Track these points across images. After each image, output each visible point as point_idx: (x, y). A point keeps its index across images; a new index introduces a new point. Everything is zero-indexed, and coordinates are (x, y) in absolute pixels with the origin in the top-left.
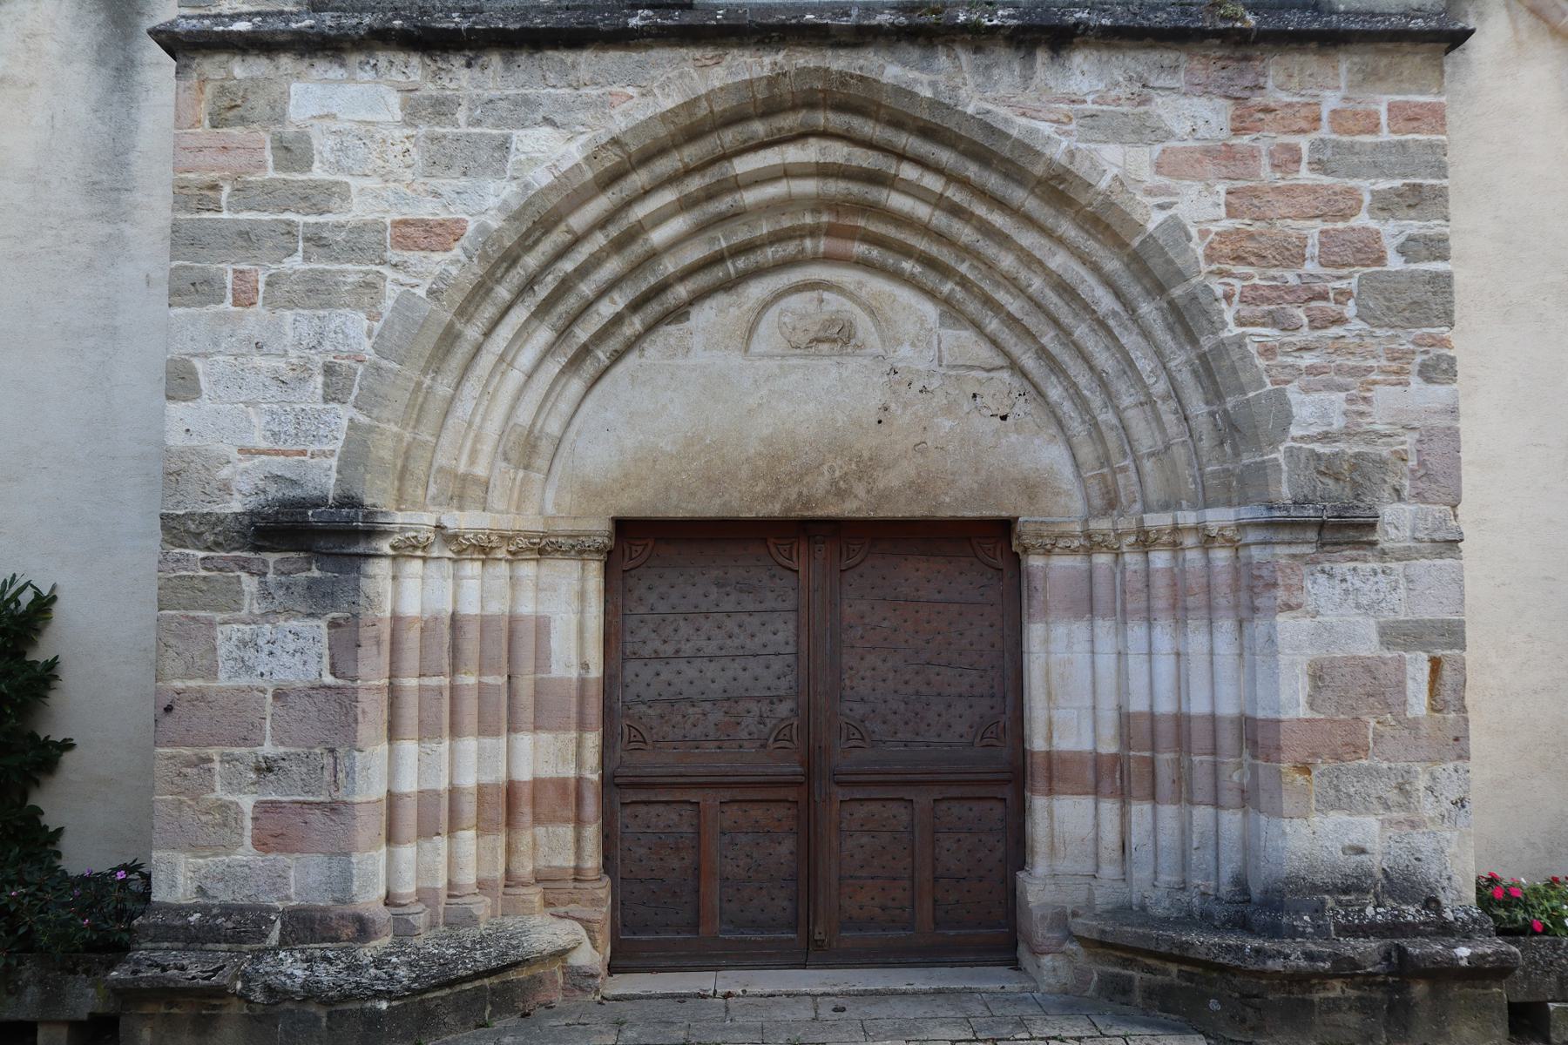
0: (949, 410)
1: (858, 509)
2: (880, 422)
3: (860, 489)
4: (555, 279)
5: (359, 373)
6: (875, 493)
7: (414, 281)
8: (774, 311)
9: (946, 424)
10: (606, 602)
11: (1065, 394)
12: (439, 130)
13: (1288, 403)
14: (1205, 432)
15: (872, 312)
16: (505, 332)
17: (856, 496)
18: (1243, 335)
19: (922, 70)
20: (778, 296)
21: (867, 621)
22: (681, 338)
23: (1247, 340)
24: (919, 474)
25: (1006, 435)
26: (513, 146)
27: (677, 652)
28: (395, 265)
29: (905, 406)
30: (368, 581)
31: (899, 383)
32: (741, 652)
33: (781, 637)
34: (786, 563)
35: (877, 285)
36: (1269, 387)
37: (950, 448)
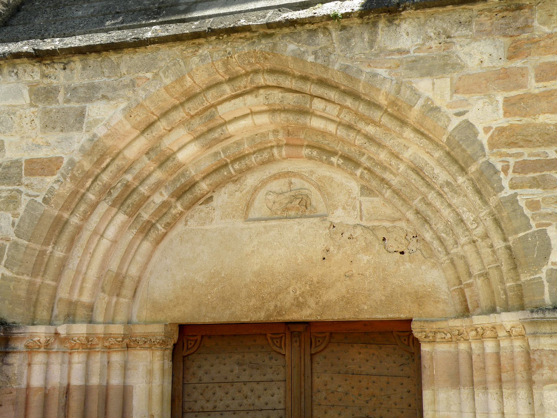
0: (367, 249)
1: (311, 315)
2: (324, 259)
3: (311, 302)
4: (122, 185)
5: (7, 247)
6: (321, 304)
7: (36, 193)
8: (263, 192)
9: (365, 258)
10: (173, 376)
11: (434, 236)
12: (49, 107)
13: (549, 239)
14: (503, 260)
15: (319, 188)
16: (95, 218)
17: (309, 307)
18: (516, 194)
19: (309, 44)
20: (264, 183)
21: (328, 387)
22: (208, 213)
23: (518, 198)
24: (348, 293)
25: (403, 265)
26: (87, 113)
27: (215, 407)
28: (27, 185)
29: (339, 247)
30: (8, 367)
31: (336, 233)
32: (252, 408)
33: (275, 398)
34: (278, 350)
35: (323, 171)
36: (534, 229)
37: (367, 273)
